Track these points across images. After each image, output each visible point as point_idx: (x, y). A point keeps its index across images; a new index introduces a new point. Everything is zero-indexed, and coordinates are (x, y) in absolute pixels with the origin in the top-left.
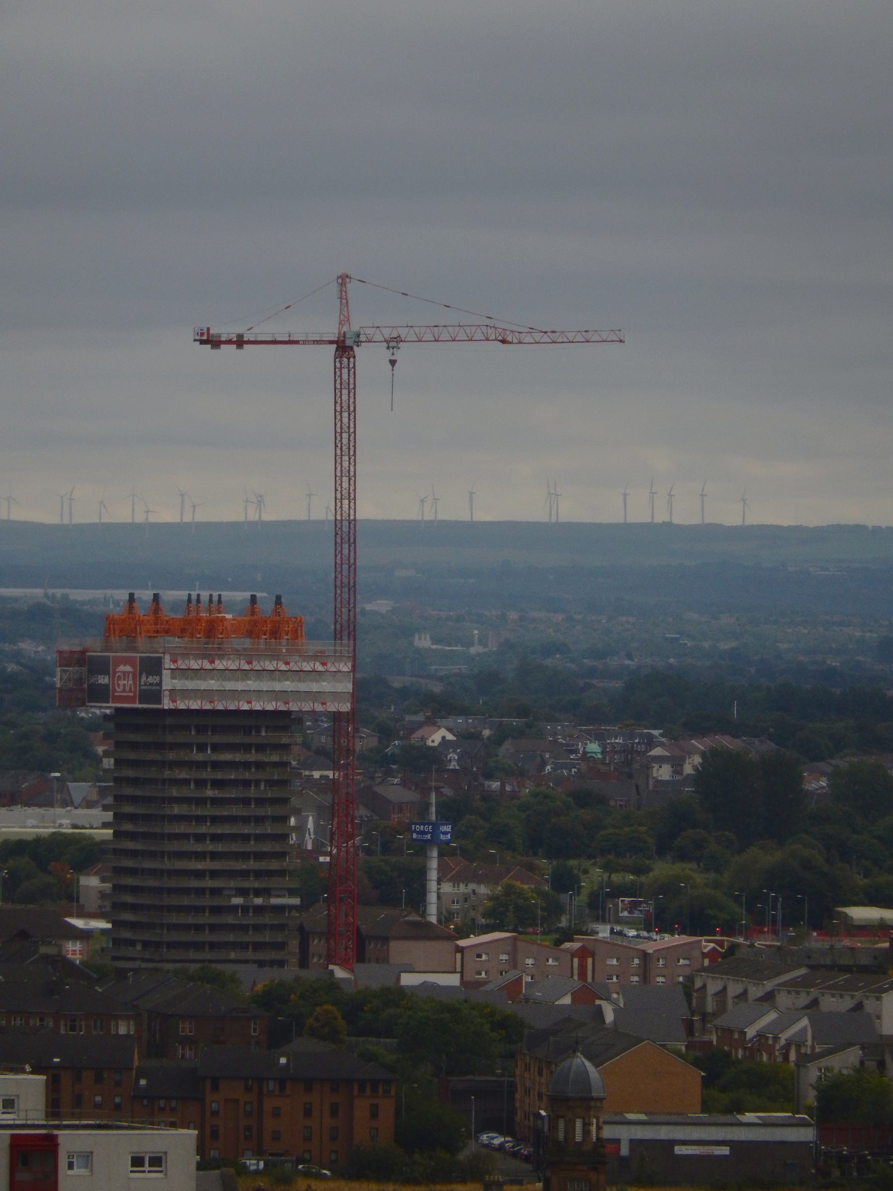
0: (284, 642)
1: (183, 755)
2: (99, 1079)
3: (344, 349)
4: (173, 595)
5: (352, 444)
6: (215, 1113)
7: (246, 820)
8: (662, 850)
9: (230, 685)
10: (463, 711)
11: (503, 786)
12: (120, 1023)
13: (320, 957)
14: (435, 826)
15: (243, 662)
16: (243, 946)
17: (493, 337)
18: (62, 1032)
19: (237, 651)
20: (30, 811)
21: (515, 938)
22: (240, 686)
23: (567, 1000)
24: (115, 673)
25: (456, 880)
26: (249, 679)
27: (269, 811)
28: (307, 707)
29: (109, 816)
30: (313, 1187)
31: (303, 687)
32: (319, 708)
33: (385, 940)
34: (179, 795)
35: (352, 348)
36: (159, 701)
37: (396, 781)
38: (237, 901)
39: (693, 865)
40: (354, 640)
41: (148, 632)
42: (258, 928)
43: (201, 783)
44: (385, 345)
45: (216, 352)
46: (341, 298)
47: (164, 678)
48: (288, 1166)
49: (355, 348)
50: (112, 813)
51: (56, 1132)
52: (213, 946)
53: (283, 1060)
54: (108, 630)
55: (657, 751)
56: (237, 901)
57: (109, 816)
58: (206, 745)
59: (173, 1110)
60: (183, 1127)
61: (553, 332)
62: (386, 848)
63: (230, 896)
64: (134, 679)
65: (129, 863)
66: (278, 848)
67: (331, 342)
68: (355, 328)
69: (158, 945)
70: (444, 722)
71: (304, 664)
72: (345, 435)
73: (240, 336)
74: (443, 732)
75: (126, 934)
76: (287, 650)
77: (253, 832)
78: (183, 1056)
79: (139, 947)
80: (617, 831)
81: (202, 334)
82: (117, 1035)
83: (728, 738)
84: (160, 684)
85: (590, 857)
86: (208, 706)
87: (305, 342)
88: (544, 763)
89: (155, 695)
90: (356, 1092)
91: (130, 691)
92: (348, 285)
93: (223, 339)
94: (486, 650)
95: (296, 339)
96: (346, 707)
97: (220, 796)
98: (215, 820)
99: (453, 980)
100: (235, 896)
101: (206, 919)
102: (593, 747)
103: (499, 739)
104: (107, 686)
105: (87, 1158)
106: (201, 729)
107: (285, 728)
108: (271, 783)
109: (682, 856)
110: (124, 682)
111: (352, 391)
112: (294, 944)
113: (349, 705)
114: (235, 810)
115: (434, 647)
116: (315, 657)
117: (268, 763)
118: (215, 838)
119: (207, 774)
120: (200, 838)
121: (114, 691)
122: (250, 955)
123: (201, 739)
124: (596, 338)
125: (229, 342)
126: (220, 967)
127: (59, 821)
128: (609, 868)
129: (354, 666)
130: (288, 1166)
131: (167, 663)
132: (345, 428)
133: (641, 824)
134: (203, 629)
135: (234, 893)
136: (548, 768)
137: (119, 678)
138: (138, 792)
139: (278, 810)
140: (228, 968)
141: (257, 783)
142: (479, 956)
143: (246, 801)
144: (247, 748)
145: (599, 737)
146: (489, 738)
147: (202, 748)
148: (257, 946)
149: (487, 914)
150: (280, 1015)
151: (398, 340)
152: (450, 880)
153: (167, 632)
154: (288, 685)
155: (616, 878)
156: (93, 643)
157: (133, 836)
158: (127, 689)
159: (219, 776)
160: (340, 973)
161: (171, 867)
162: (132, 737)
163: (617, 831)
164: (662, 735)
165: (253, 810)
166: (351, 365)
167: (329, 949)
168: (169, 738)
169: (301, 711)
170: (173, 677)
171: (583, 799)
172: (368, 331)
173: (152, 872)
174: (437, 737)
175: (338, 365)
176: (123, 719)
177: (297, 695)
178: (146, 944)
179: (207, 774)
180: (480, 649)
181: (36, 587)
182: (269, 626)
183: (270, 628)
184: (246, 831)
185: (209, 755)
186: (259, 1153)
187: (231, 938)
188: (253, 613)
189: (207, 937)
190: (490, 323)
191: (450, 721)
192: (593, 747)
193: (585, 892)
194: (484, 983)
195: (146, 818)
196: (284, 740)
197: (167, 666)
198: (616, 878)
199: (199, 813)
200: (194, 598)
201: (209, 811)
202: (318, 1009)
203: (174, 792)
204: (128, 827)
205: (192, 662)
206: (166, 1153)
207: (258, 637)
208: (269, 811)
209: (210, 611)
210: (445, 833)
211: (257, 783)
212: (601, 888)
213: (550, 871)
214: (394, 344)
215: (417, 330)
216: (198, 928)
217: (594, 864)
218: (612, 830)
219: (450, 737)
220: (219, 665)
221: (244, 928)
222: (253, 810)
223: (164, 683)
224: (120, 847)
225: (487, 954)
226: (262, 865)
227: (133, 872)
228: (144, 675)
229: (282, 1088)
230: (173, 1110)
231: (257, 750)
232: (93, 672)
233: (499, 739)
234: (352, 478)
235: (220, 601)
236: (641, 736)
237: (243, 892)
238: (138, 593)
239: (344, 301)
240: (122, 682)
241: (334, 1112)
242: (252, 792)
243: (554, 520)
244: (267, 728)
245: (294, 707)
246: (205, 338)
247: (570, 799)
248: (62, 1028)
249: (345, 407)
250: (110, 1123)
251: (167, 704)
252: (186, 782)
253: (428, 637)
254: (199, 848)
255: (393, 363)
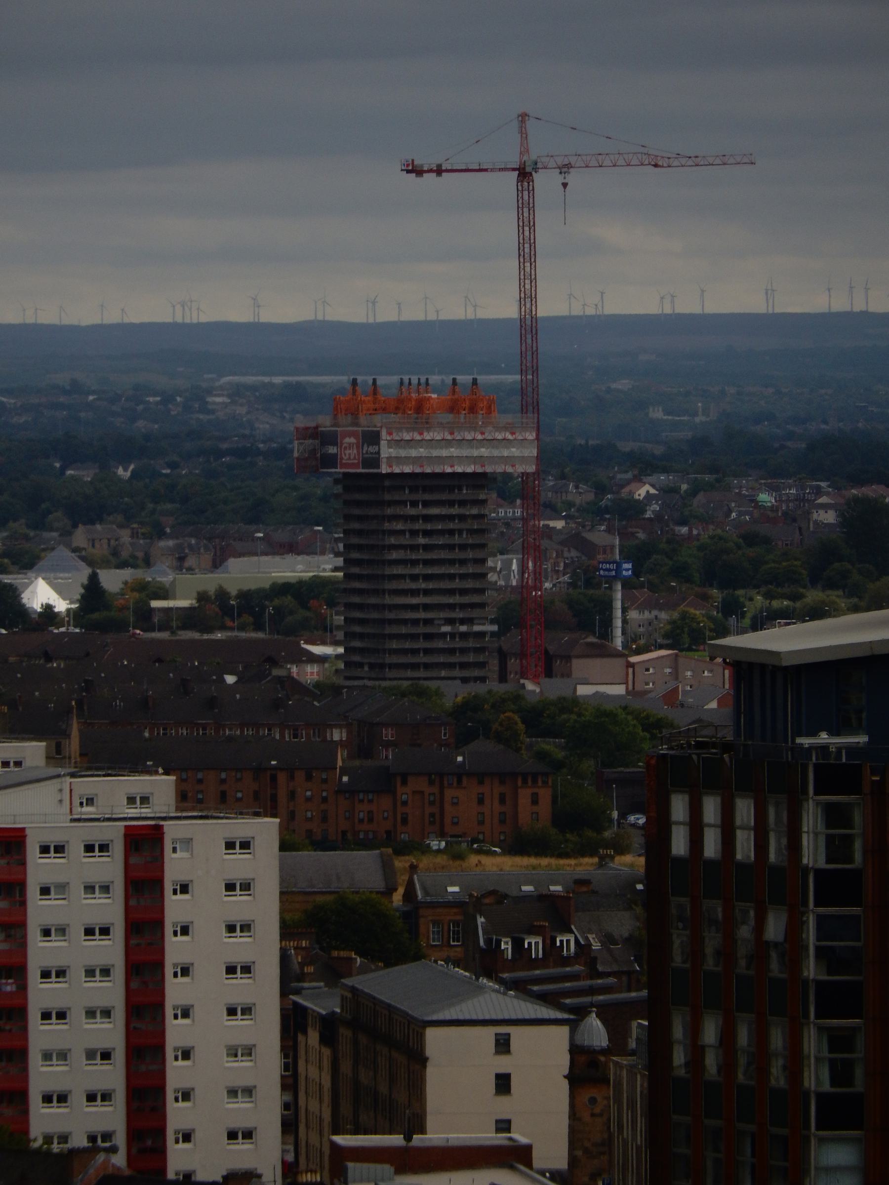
0: (480, 416)
1: (399, 511)
2: (309, 778)
3: (524, 174)
4: (388, 381)
5: (533, 253)
6: (405, 803)
7: (452, 562)
8: (815, 580)
9: (435, 453)
10: (665, 470)
11: (690, 530)
12: (334, 730)
13: (516, 673)
14: (619, 566)
15: (446, 434)
16: (451, 666)
17: (647, 162)
18: (287, 739)
19: (441, 424)
20: (300, 558)
21: (676, 655)
22: (444, 453)
23: (713, 705)
24: (342, 444)
25: (641, 608)
26: (452, 447)
27: (470, 554)
28: (499, 469)
29: (340, 561)
30: (483, 862)
31: (496, 453)
32: (510, 470)
33: (568, 658)
34: (397, 543)
35: (531, 174)
36: (378, 466)
37: (603, 528)
38: (446, 629)
39: (840, 593)
40: (538, 414)
41: (368, 410)
42: (463, 651)
43: (414, 533)
44: (558, 170)
45: (419, 179)
46: (521, 132)
47: (382, 448)
48: (464, 845)
49: (533, 173)
50: (342, 559)
51: (162, 823)
52: (427, 666)
53: (460, 759)
54: (336, 409)
55: (823, 500)
56: (446, 629)
57: (340, 561)
58: (418, 502)
59: (371, 801)
60: (266, 816)
61: (696, 157)
62: (589, 583)
63: (440, 625)
64: (358, 447)
65: (356, 599)
66: (478, 585)
67: (514, 169)
68: (534, 157)
69: (382, 666)
70: (649, 479)
71: (497, 434)
72: (527, 246)
73: (439, 166)
74: (647, 487)
75: (357, 658)
76: (483, 423)
77: (457, 572)
78: (387, 757)
79: (366, 668)
80: (777, 566)
81: (408, 165)
82: (332, 741)
83: (883, 487)
84: (378, 453)
85: (756, 587)
86: (418, 470)
87: (492, 170)
88: (730, 511)
89: (374, 461)
90: (520, 783)
91: (355, 458)
92: (527, 122)
93: (425, 169)
94: (708, 419)
95: (485, 167)
96: (531, 469)
97: (431, 542)
98: (426, 563)
99: (619, 690)
100: (444, 625)
101: (421, 644)
102: (765, 498)
103: (694, 492)
104: (336, 455)
105: (188, 842)
106: (413, 489)
107: (482, 487)
108: (471, 532)
109: (830, 585)
110: (349, 453)
111: (532, 209)
112: (494, 664)
113: (534, 467)
114: (443, 555)
115: (665, 417)
116: (505, 428)
117: (469, 516)
118: (427, 578)
119: (419, 525)
120: (414, 578)
121: (342, 459)
122: (457, 673)
123: (414, 497)
124: (732, 161)
125: (430, 171)
126: (426, 683)
127: (322, 567)
128: (769, 596)
129: (537, 435)
130: (464, 845)
131: (384, 434)
132: (527, 239)
133: (796, 559)
134: (412, 408)
135: (443, 622)
136: (734, 515)
137: (345, 448)
138: (363, 541)
139: (479, 554)
140: (433, 685)
141: (460, 532)
142: (647, 670)
143: (451, 547)
144: (451, 503)
145: (772, 488)
146: (686, 491)
147: (414, 504)
148: (463, 666)
149: (666, 636)
150: (469, 722)
151: (569, 166)
152: (635, 609)
153: (384, 410)
154: (484, 451)
155: (776, 604)
156: (325, 421)
157: (359, 577)
158: (352, 457)
159: (429, 527)
160: (530, 686)
161: (392, 603)
162: (358, 496)
163: (777, 566)
164: (829, 486)
165: (457, 554)
166: (531, 188)
167: (522, 667)
168: (387, 497)
169: (494, 473)
170: (389, 447)
171: (751, 539)
172: (544, 159)
173: (376, 607)
174: (642, 491)
175: (520, 188)
176: (350, 481)
177: (492, 460)
178: (372, 666)
179: (419, 525)
180: (703, 419)
181: (343, 375)
182: (467, 403)
183: (468, 405)
184: (452, 571)
185: (420, 510)
186: (442, 835)
187: (441, 659)
188: (454, 392)
189: (422, 659)
190: (645, 150)
191: (653, 479)
192: (765, 498)
193: (749, 615)
194: (646, 692)
195: (370, 562)
196: (482, 497)
197: (384, 438)
198: (776, 604)
199: (414, 557)
200: (406, 381)
201: (422, 555)
202: (502, 716)
203: (393, 540)
204: (355, 570)
205: (405, 434)
206: (253, 838)
207: (459, 413)
208: (470, 554)
209: (419, 392)
210: (627, 570)
211: (460, 532)
212: (761, 612)
213: (720, 600)
214: (566, 170)
215: (626, 156)
216: (414, 652)
217: (758, 593)
218: (773, 565)
219: (653, 491)
220: (427, 436)
221: (452, 651)
222: (457, 554)
223: (382, 452)
224: (349, 587)
225: (654, 668)
226: (466, 599)
227: (360, 607)
228: (365, 446)
229: (460, 782)
230: (371, 801)
231: (459, 506)
232: (324, 443)
233: (694, 492)
234: (533, 280)
235: (427, 384)
236: (811, 487)
237: (450, 621)
238: (360, 379)
239: (524, 136)
240: (347, 452)
241: (502, 799)
242: (456, 540)
243: (770, 311)
244: (467, 487)
245: (489, 469)
246: (410, 168)
247: (741, 540)
248: (287, 736)
249: (526, 223)
250: (210, 814)
251: (384, 469)
252: (402, 532)
253: (660, 409)
254: (413, 586)
255: (565, 185)
